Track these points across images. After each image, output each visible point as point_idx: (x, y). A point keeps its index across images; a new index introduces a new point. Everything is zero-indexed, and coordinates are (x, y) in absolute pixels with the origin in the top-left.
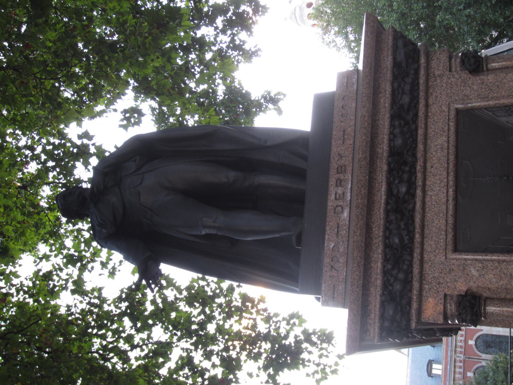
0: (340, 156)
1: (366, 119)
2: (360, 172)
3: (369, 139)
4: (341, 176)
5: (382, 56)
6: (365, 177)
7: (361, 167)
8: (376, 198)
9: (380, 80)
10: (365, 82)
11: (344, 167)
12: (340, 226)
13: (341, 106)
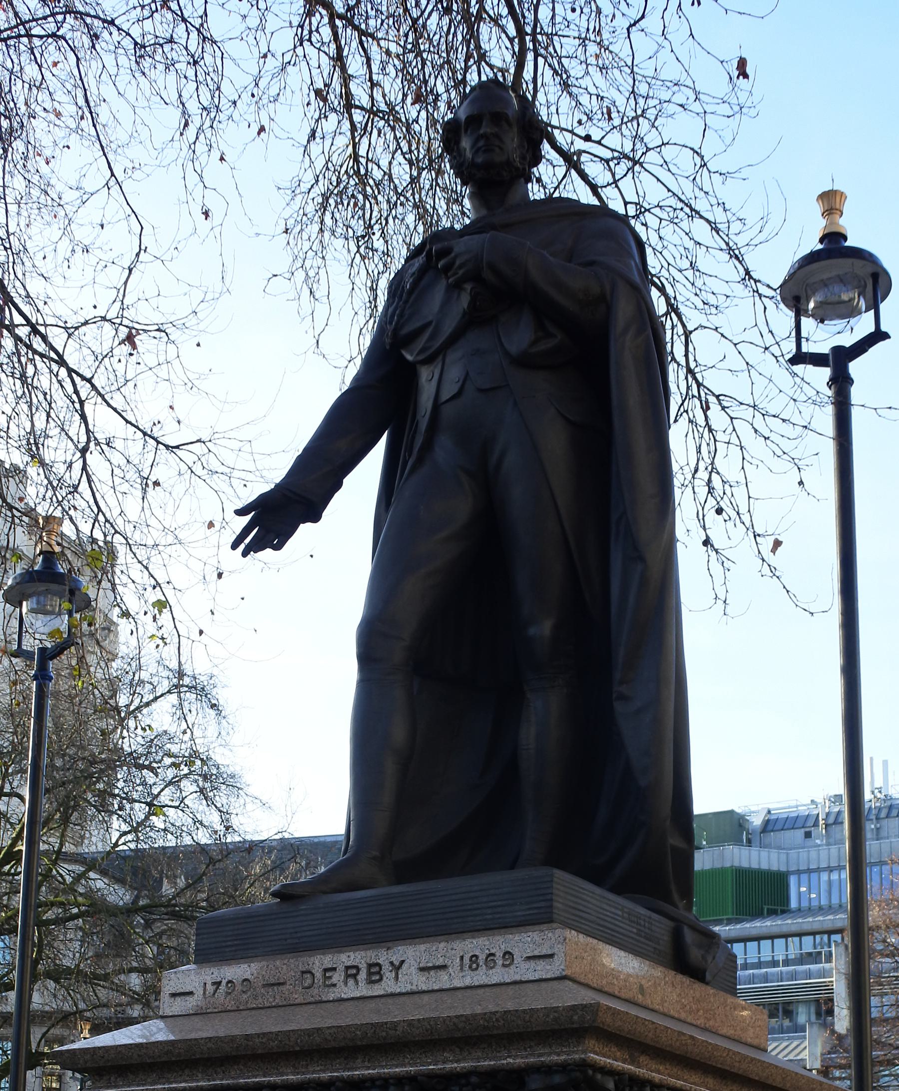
0: (396, 968)
1: (391, 1032)
2: (300, 1035)
3: (359, 1043)
4: (363, 975)
5: (532, 1044)
6: (297, 1043)
7: (309, 1036)
8: (282, 1064)
9: (486, 1046)
10: (455, 1020)
11: (378, 977)
12: (281, 988)
13: (493, 951)
